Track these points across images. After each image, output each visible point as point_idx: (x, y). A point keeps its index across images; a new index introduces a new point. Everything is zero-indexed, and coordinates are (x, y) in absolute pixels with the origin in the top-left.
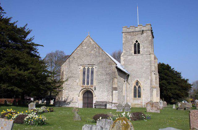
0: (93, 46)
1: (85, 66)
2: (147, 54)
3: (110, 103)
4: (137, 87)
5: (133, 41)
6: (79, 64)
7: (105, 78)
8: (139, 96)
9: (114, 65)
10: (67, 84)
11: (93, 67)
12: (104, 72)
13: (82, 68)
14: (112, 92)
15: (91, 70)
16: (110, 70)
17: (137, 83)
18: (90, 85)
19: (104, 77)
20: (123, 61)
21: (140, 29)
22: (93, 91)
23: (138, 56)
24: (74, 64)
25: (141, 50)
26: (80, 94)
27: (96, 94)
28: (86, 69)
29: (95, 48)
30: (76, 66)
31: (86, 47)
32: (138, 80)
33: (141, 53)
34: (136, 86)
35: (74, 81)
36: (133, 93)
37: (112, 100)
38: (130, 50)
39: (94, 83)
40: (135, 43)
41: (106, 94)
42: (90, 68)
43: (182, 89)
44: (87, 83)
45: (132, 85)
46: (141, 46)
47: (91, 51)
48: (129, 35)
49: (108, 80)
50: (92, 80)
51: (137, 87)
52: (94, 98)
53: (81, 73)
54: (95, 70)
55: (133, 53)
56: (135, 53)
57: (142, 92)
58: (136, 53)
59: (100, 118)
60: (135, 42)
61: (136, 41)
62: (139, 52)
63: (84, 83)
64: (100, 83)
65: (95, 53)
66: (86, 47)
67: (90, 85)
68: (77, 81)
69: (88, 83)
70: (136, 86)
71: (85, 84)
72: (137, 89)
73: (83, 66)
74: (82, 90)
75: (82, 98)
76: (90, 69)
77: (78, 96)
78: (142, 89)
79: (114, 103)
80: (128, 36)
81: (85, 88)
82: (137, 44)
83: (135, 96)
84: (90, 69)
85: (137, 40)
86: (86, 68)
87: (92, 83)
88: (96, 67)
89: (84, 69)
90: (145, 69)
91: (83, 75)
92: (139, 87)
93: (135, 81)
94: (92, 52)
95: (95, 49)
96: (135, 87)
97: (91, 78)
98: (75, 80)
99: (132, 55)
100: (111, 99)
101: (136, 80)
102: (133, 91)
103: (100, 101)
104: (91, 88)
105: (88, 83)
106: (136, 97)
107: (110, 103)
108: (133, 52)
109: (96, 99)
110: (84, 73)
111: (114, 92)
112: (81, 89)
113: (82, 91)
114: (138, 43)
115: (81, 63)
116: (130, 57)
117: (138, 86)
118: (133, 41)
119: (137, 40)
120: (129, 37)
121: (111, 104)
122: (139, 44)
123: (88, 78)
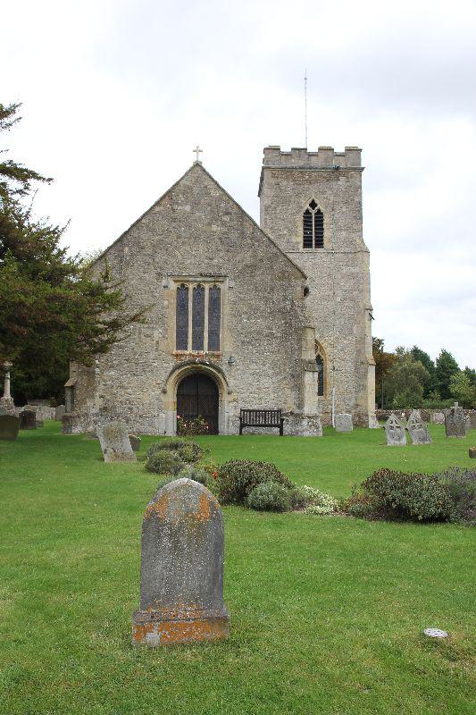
2: (346, 250)
13: (173, 286)
15: (210, 294)
16: (285, 298)
21: (326, 160)
22: (223, 374)
25: (327, 234)
27: (232, 382)
30: (150, 276)
31: (188, 208)
40: (307, 212)
42: (207, 287)
46: (326, 220)
47: (209, 224)
50: (214, 334)
53: (169, 305)
54: (227, 297)
55: (302, 245)
56: (307, 244)
58: (310, 246)
59: (420, 517)
60: (307, 206)
62: (320, 243)
63: (182, 343)
68: (157, 334)
69: (198, 345)
75: (176, 400)
80: (284, 183)
82: (313, 212)
85: (313, 201)
86: (191, 287)
87: (214, 344)
88: (233, 284)
89: (183, 289)
91: (178, 314)
94: (214, 228)
95: (226, 218)
98: (149, 332)
104: (213, 360)
105: (198, 345)
108: (301, 239)
110: (182, 307)
113: (177, 372)
114: (319, 211)
119: (313, 201)
120: (287, 185)
122: (319, 214)
123: (198, 323)
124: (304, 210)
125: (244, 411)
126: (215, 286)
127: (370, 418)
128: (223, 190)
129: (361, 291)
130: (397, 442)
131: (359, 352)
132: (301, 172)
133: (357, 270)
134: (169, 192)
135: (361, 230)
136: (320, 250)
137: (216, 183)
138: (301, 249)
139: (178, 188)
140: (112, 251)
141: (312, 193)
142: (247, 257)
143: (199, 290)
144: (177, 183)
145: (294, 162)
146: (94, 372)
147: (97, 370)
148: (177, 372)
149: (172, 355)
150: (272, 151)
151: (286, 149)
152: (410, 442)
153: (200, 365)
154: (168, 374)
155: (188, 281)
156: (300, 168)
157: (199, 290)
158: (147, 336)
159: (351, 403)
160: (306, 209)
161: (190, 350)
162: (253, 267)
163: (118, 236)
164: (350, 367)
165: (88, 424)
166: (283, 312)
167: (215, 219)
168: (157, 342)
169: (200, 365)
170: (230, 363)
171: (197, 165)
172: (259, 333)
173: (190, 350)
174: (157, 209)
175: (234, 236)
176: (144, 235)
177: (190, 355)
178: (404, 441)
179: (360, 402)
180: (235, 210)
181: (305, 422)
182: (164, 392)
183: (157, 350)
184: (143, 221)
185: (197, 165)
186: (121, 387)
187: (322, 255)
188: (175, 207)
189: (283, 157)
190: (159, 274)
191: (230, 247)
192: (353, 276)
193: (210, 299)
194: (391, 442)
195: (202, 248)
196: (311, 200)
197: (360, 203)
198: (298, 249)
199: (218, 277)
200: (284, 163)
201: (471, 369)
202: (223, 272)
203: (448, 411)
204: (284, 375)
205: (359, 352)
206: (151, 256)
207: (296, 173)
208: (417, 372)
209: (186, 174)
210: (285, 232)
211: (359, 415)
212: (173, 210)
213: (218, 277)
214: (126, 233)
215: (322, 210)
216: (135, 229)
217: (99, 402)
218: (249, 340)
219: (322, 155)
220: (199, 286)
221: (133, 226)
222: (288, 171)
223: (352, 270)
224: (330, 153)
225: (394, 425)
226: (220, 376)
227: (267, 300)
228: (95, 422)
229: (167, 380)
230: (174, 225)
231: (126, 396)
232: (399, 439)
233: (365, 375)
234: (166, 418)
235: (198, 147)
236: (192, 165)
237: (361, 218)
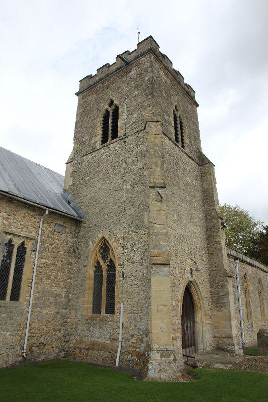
4: (105, 267)
8: (111, 309)
17: (105, 248)
33: (121, 133)
34: (101, 262)
38: (92, 135)
45: (86, 259)
46: (120, 111)
51: (105, 267)
60: (107, 107)
62: (115, 135)
70: (101, 262)
92: (112, 267)
93: (97, 240)
96: (98, 268)
101: (100, 236)
102: (90, 283)
106: (4, 298)
108: (99, 138)
193: (108, 276)
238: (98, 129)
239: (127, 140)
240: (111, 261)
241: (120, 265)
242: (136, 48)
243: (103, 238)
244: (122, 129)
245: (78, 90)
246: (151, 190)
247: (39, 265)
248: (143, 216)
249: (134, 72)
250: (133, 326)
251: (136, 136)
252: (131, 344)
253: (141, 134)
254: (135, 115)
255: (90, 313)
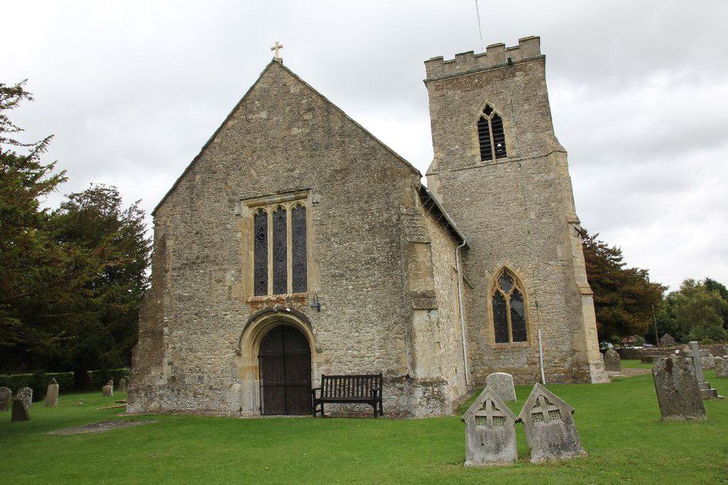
0: (299, 104)
1: (261, 201)
3: (399, 380)
4: (507, 297)
5: (474, 108)
6: (234, 193)
7: (368, 251)
8: (521, 335)
9: (409, 181)
10: (180, 298)
11: (303, 202)
12: (356, 220)
13: (248, 213)
14: (408, 320)
16: (389, 206)
17: (506, 276)
18: (290, 293)
19: (362, 247)
20: (439, 193)
21: (497, 58)
22: (309, 324)
23: (501, 169)
24: (213, 198)
26: (244, 346)
28: (270, 217)
29: (310, 110)
30: (222, 206)
31: (264, 115)
32: (510, 266)
35: (213, 280)
36: (493, 322)
37: (413, 366)
38: (464, 146)
39: (309, 280)
40: (482, 119)
41: (373, 333)
43: (634, 304)
44: (275, 283)
46: (505, 124)
47: (289, 128)
48: (454, 88)
49: (380, 256)
50: (300, 269)
51: (507, 297)
52: (316, 359)
54: (312, 216)
55: (479, 158)
56: (486, 155)
57: (532, 317)
58: (490, 157)
60: (481, 113)
61: (483, 107)
62: (501, 153)
63: (260, 287)
64: (342, 275)
65: (308, 134)
66: (264, 115)
67: (290, 293)
69: (280, 286)
71: (266, 293)
72: (508, 303)
73: (251, 202)
74: (254, 319)
75: (256, 363)
76: (289, 214)
77: (231, 354)
78: (529, 301)
79: (425, 384)
80: (450, 93)
81: (269, 311)
82: (489, 118)
83: (501, 336)
84: (289, 214)
86: (269, 210)
87: (301, 284)
88: (318, 197)
89: (260, 216)
90: (533, 216)
92: (517, 296)
94: (295, 131)
95: (307, 117)
96: (498, 297)
97: (294, 255)
98: (219, 275)
99: (472, 166)
100: (406, 360)
101: (499, 266)
102: (490, 314)
103: (349, 372)
104: (296, 305)
105: (280, 286)
106: (507, 340)
107: (399, 380)
108: (477, 151)
109: (327, 361)
110: (260, 237)
111: (420, 319)
112: (246, 317)
113: (254, 325)
114: (496, 116)
115: (242, 192)
116: (464, 176)
117: (511, 291)
118: (474, 108)
120: (456, 95)
121: (406, 385)
122: (497, 121)
123: (280, 257)
124: (477, 118)
125: (328, 378)
126: (299, 205)
127: (593, 368)
128: (304, 83)
129: (560, 201)
130: (490, 457)
131: (568, 280)
132: (469, 77)
133: (552, 175)
134: (244, 100)
135: (551, 128)
136: (502, 160)
137: (295, 77)
138: (479, 164)
139: (253, 93)
140: (183, 182)
141: (485, 97)
142: (334, 159)
143: (280, 215)
144: (252, 88)
145: (458, 68)
146: (162, 333)
147: (166, 330)
148: (254, 325)
149: (247, 302)
150: (435, 62)
151: (449, 57)
152: (524, 455)
153: (280, 314)
154: (242, 329)
155: (264, 204)
156: (468, 72)
157: (280, 215)
158: (219, 281)
159: (566, 348)
160: (479, 115)
161: (271, 295)
162: (344, 171)
163: (188, 164)
164: (558, 300)
165: (151, 400)
166: (386, 226)
167: (297, 119)
168: (230, 288)
169: (280, 314)
170: (318, 308)
171: (277, 63)
172: (355, 261)
173: (271, 295)
174: (231, 123)
175: (319, 136)
176: (217, 158)
177: (269, 301)
178: (510, 452)
179: (579, 346)
180: (320, 102)
181: (419, 392)
182: (239, 354)
183: (229, 298)
184: (216, 140)
185: (277, 63)
186: (191, 350)
187: (505, 166)
188: (250, 116)
189: (447, 66)
190: (231, 201)
191: (312, 148)
192: (549, 184)
193: (294, 222)
194: (477, 457)
195: (280, 157)
196: (484, 105)
197: (546, 96)
198: (475, 163)
199: (300, 193)
200: (448, 71)
201: (710, 278)
202: (305, 185)
203: (659, 364)
204: (395, 318)
205: (568, 280)
206: (225, 181)
207: (463, 80)
208: (715, 303)
209: (262, 75)
210: (457, 147)
211: (577, 364)
212: (248, 120)
213: (300, 193)
214: (197, 158)
215: (500, 113)
216: (207, 152)
217: (167, 370)
218: (341, 271)
219: (494, 52)
220: (280, 208)
221: (205, 148)
222: (453, 81)
223: (546, 177)
224: (501, 49)
225: (489, 413)
226: (305, 326)
227: (364, 212)
228: (161, 396)
229: (241, 337)
230: (249, 137)
231: (196, 363)
232: (498, 450)
233: (578, 310)
234: (240, 391)
235: (277, 43)
236: (270, 61)
237: (549, 114)
238: (474, 140)
239: (523, 163)
240: (516, 291)
241: (531, 295)
242: (517, 44)
243: (506, 270)
244: (513, 148)
245: (426, 78)
246: (569, 225)
247: (546, 348)
248: (555, 249)
249: (519, 78)
250: (554, 349)
251: (534, 161)
252: (553, 364)
253: (542, 161)
254: (529, 136)
255: (493, 344)
